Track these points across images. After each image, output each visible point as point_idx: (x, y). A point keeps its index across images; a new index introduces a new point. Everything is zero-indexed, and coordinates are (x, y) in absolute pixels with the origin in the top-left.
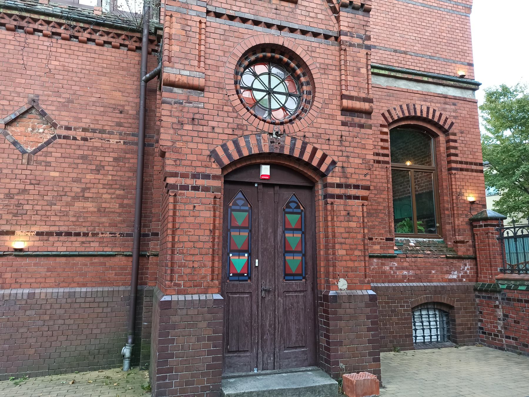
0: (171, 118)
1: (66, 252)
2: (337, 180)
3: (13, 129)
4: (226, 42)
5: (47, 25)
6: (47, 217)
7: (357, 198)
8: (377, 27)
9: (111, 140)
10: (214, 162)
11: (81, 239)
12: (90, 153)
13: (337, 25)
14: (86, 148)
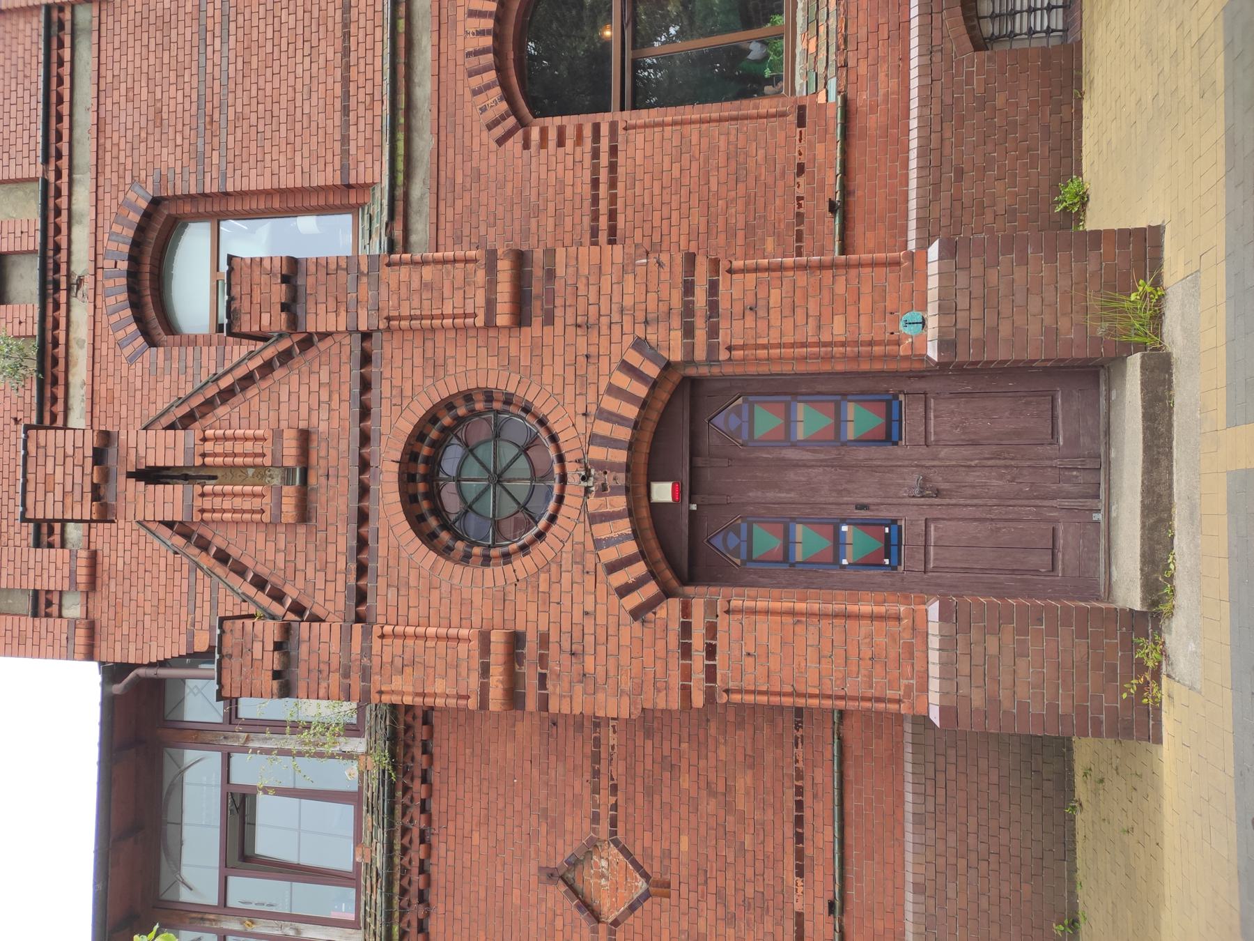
0: (574, 697)
1: (834, 827)
2: (677, 335)
3: (605, 909)
4: (411, 584)
5: (410, 851)
6: (768, 857)
7: (713, 287)
8: (298, 161)
9: (611, 743)
10: (655, 613)
11: (807, 799)
12: (639, 782)
13: (337, 338)
14: (631, 788)
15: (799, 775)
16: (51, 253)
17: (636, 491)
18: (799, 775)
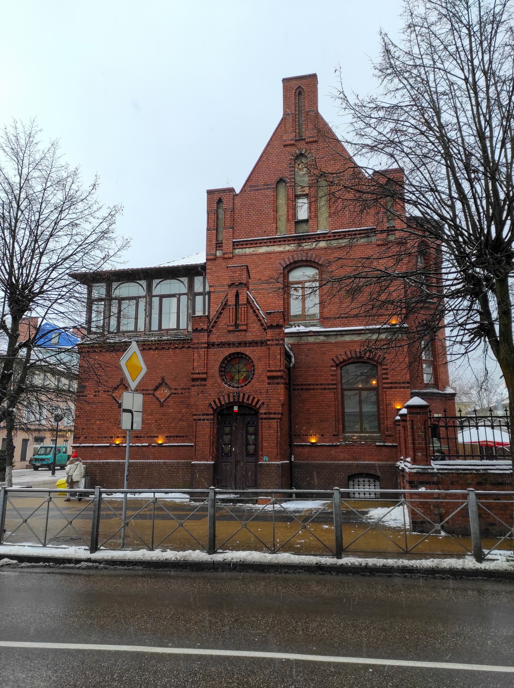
7: (274, 419)
15: (187, 437)
16: (278, 240)
17: (235, 403)
18: (187, 437)
